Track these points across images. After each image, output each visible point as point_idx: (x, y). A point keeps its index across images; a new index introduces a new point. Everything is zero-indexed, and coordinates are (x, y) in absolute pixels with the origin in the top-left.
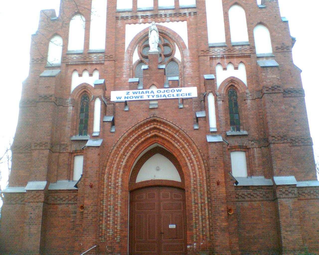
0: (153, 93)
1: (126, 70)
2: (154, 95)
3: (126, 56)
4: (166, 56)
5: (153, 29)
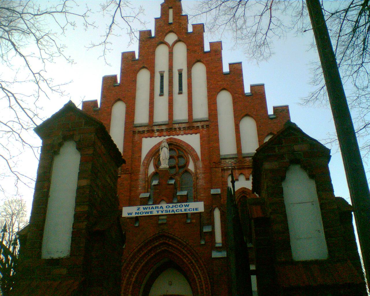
0: (162, 208)
1: (141, 183)
2: (163, 211)
3: (142, 168)
4: (180, 167)
5: (164, 146)
